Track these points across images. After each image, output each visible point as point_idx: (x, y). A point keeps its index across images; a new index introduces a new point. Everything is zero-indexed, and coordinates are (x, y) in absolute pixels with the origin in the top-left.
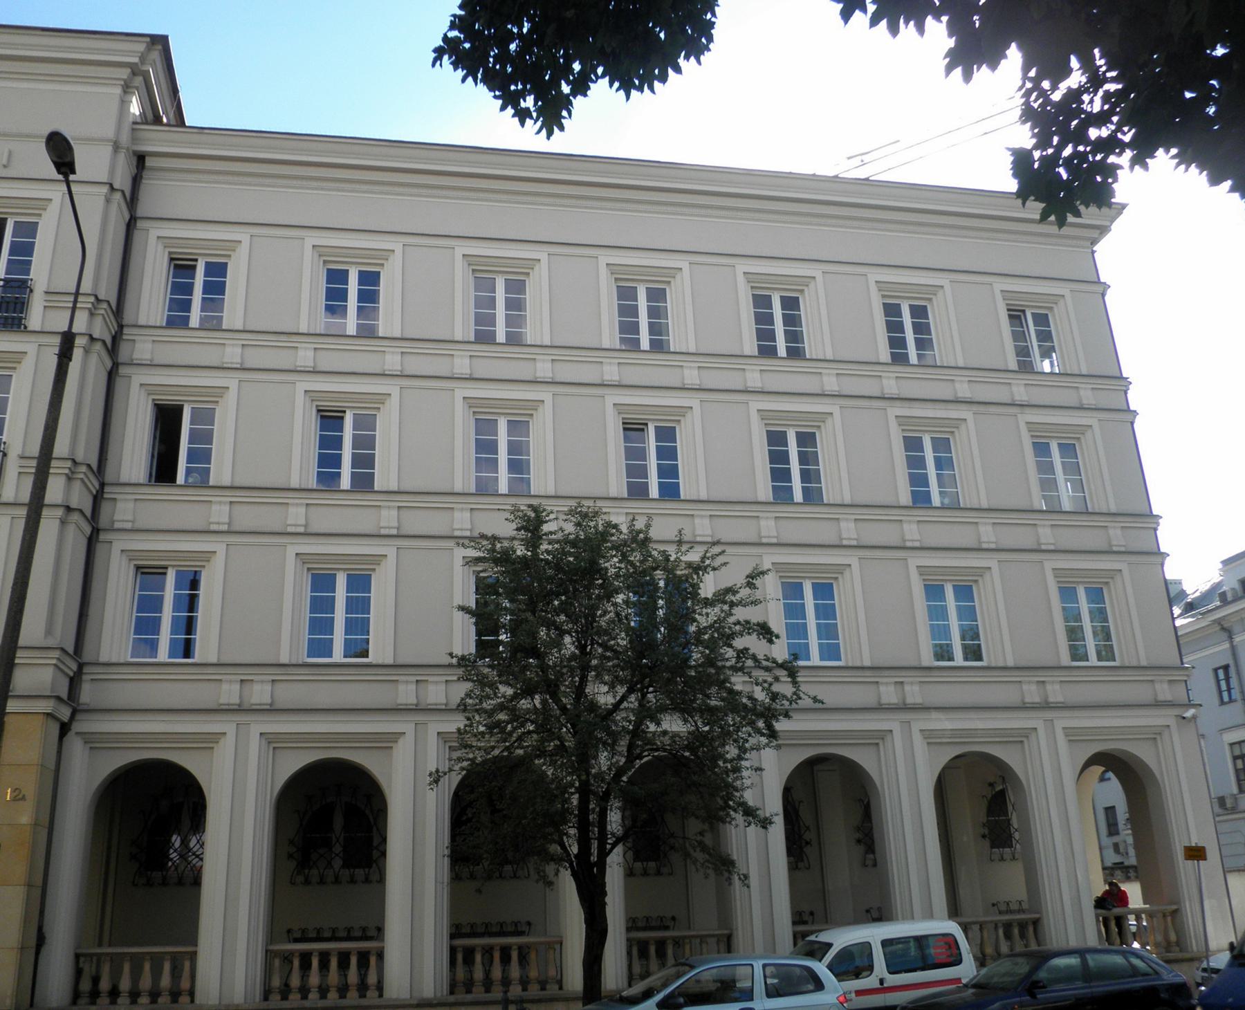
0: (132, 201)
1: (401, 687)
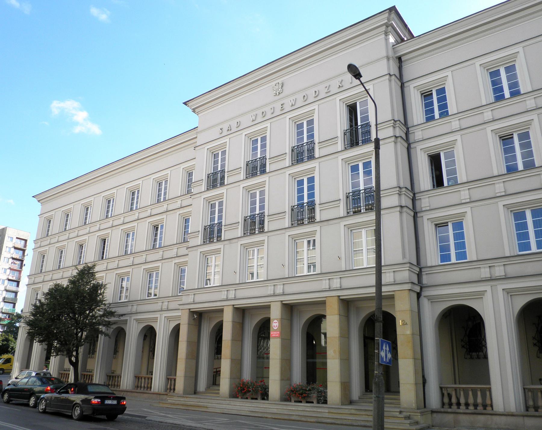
0: (401, 78)
1: (482, 270)
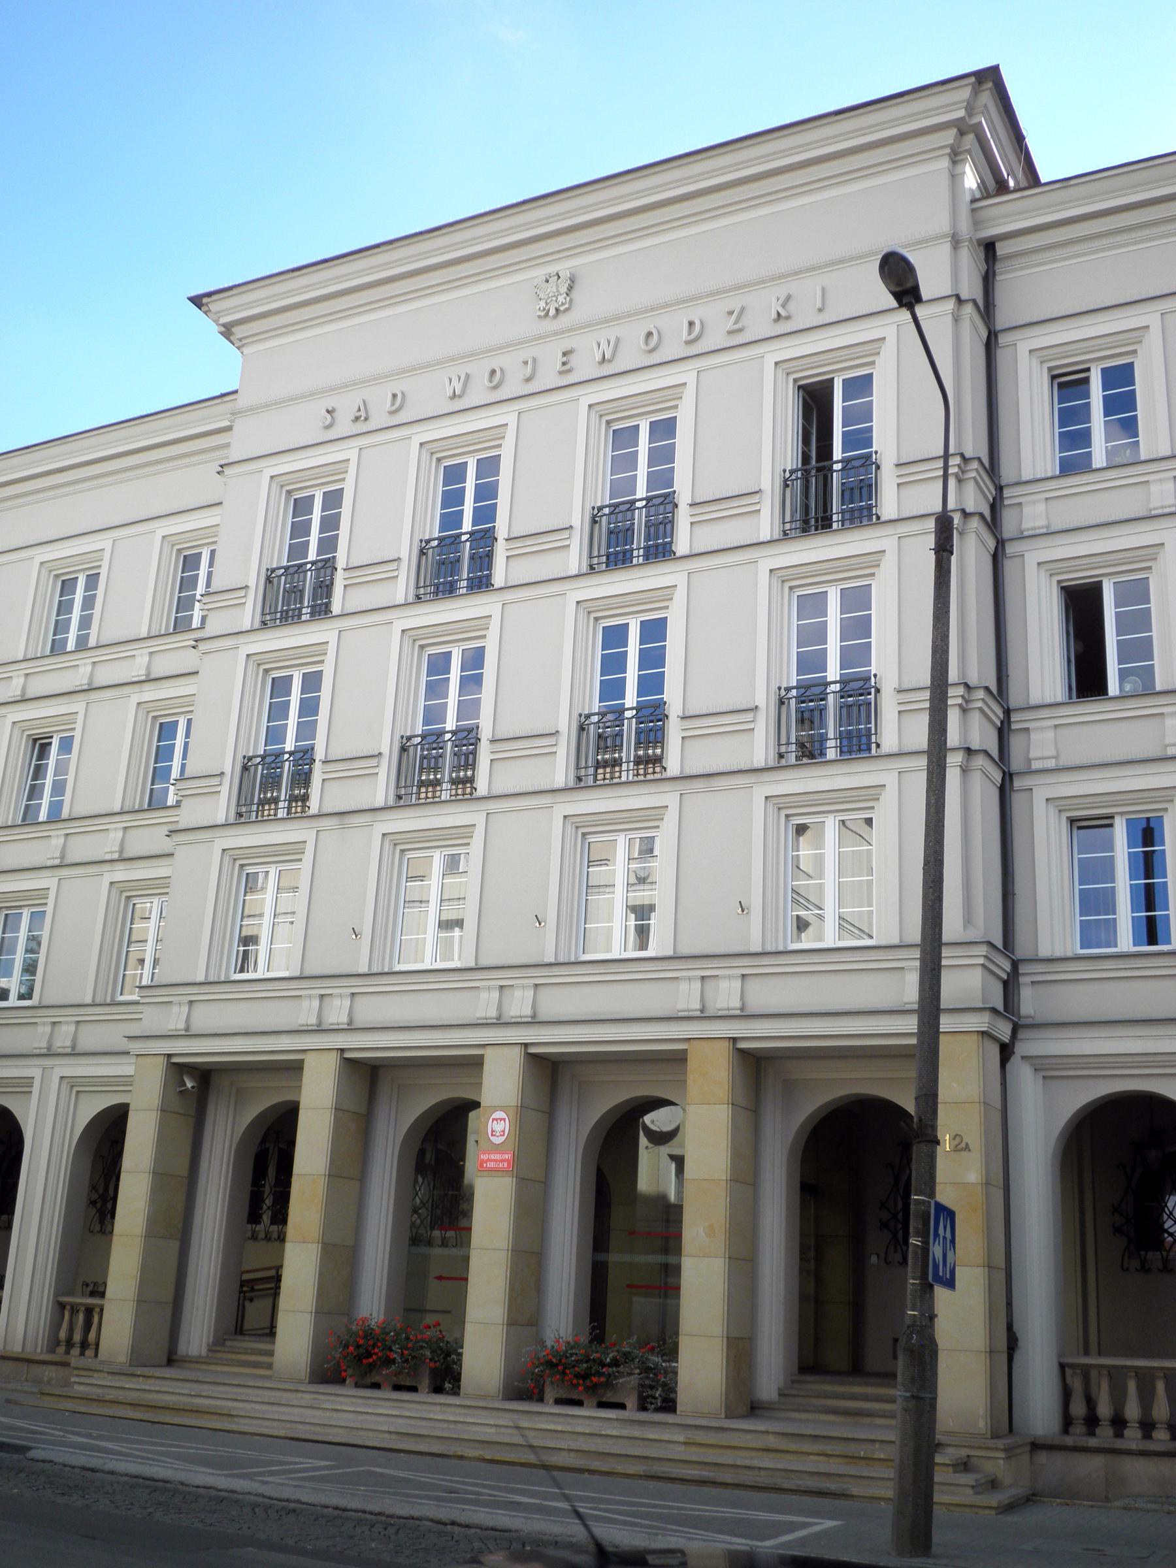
0: (987, 310)
